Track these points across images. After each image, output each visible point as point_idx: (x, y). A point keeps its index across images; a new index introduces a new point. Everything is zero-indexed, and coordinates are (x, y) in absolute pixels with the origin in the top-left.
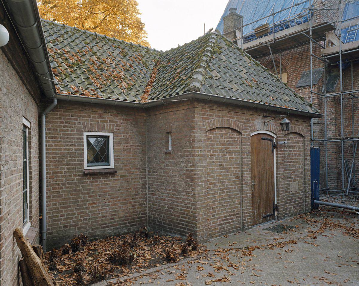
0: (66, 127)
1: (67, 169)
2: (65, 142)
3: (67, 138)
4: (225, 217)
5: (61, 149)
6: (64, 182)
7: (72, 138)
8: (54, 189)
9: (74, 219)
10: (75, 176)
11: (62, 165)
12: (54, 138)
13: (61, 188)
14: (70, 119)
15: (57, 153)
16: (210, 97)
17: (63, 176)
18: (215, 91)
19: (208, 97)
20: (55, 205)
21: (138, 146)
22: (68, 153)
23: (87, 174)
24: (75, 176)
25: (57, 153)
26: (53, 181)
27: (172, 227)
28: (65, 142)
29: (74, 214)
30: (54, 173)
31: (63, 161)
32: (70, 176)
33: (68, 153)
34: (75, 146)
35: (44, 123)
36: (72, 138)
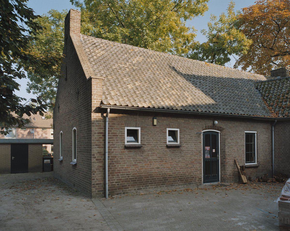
0: (284, 130)
1: (284, 147)
2: (283, 136)
3: (284, 134)
4: (80, 179)
5: (281, 139)
6: (283, 152)
7: (287, 134)
8: (278, 155)
9: (287, 168)
10: (287, 150)
11: (282, 145)
12: (278, 135)
13: (281, 155)
14: (285, 127)
15: (279, 141)
16: (190, 113)
17: (282, 150)
18: (212, 110)
19: (140, 109)
20: (279, 161)
21: (267, 138)
22: (284, 141)
23: (126, 148)
24: (287, 150)
25: (279, 141)
26: (278, 152)
27: (135, 179)
28: (283, 136)
29: (287, 166)
30: (278, 148)
31: (282, 144)
32: (286, 150)
33: (284, 141)
34: (288, 137)
35: (273, 129)
36: (287, 134)
